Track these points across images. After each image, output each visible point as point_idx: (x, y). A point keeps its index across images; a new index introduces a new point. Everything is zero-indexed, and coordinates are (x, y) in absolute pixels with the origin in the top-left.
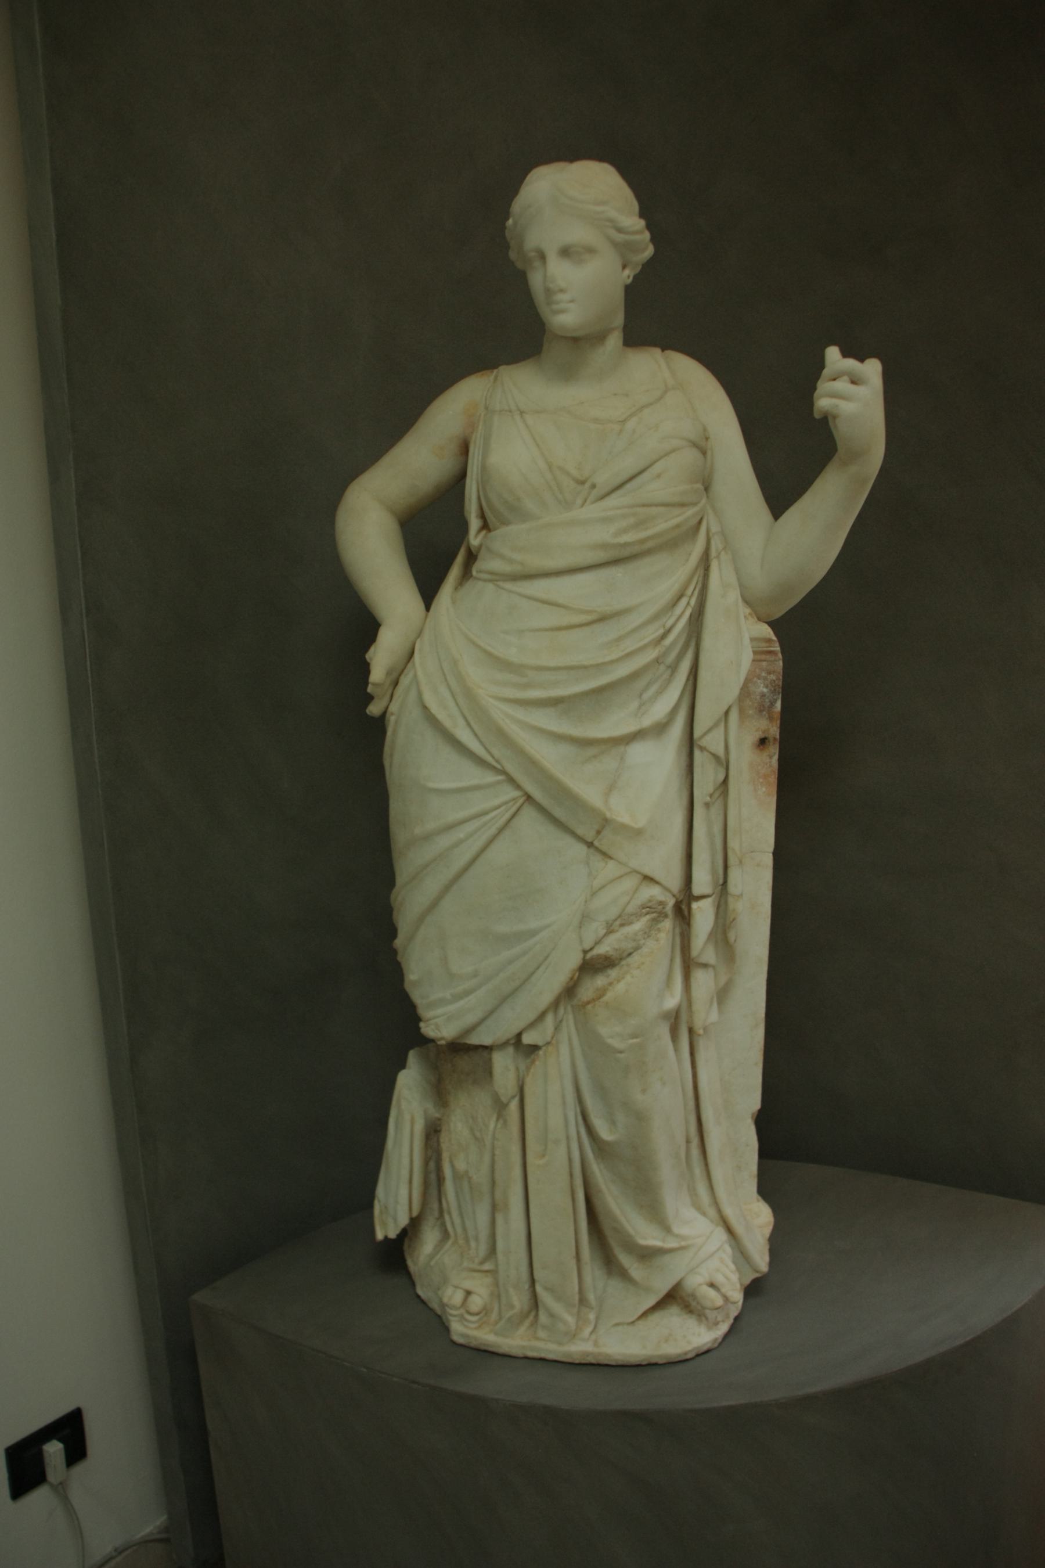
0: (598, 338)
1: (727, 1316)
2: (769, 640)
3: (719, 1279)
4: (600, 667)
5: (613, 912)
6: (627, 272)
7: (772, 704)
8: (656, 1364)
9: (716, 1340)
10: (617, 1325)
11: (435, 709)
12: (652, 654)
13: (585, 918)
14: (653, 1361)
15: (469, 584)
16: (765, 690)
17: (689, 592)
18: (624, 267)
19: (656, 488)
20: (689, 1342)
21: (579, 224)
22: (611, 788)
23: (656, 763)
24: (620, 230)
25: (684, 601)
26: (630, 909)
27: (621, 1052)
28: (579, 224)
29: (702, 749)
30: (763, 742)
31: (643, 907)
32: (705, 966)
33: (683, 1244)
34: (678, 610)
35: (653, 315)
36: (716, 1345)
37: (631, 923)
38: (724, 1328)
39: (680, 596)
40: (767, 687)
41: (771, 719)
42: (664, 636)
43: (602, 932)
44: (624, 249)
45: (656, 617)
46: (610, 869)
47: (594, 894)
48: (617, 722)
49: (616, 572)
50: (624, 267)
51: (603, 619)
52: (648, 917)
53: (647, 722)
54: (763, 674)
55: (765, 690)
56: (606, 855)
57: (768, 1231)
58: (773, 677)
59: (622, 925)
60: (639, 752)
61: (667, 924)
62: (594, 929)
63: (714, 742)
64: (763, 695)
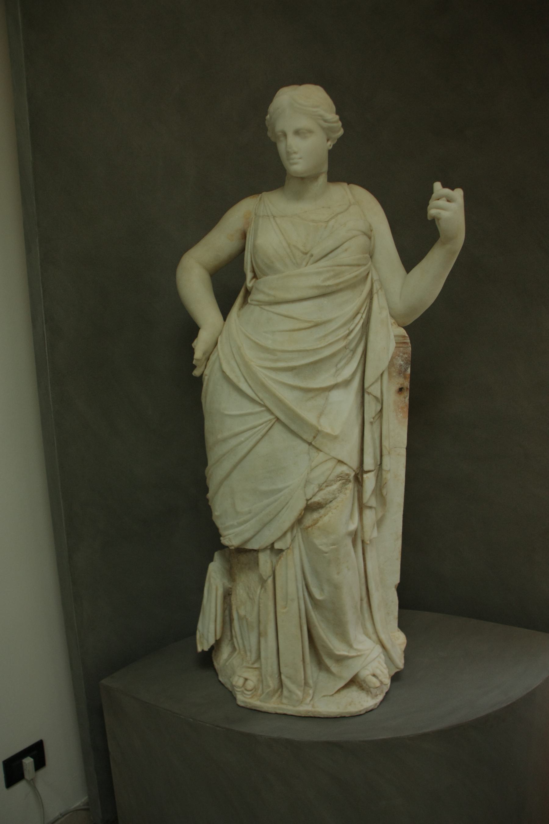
0: (314, 177)
1: (382, 692)
2: (404, 337)
3: (378, 672)
4: (315, 351)
5: (322, 479)
6: (329, 143)
7: (406, 370)
8: (344, 717)
9: (376, 704)
10: (324, 696)
11: (228, 373)
12: (343, 344)
13: (307, 482)
14: (343, 715)
15: (246, 307)
16: (402, 363)
17: (362, 311)
18: (328, 140)
19: (345, 256)
20: (362, 705)
21: (304, 117)
22: (321, 414)
23: (345, 401)
24: (326, 121)
25: (359, 316)
26: (331, 478)
27: (326, 553)
28: (304, 117)
29: (369, 394)
30: (401, 390)
31: (338, 476)
32: (370, 507)
33: (359, 653)
34: (356, 320)
35: (343, 165)
36: (376, 707)
37: (331, 485)
38: (380, 698)
39: (357, 313)
40: (403, 361)
41: (405, 378)
42: (349, 334)
43: (316, 490)
44: (328, 131)
45: (345, 324)
46: (321, 457)
47: (312, 470)
48: (324, 379)
49: (324, 301)
50: (328, 140)
51: (317, 325)
52: (340, 482)
53: (340, 379)
54: (401, 354)
55: (402, 363)
56: (318, 449)
57: (403, 647)
58: (406, 356)
59: (327, 486)
60: (336, 395)
61: (351, 486)
62: (312, 488)
63: (375, 390)
64: (401, 365)
